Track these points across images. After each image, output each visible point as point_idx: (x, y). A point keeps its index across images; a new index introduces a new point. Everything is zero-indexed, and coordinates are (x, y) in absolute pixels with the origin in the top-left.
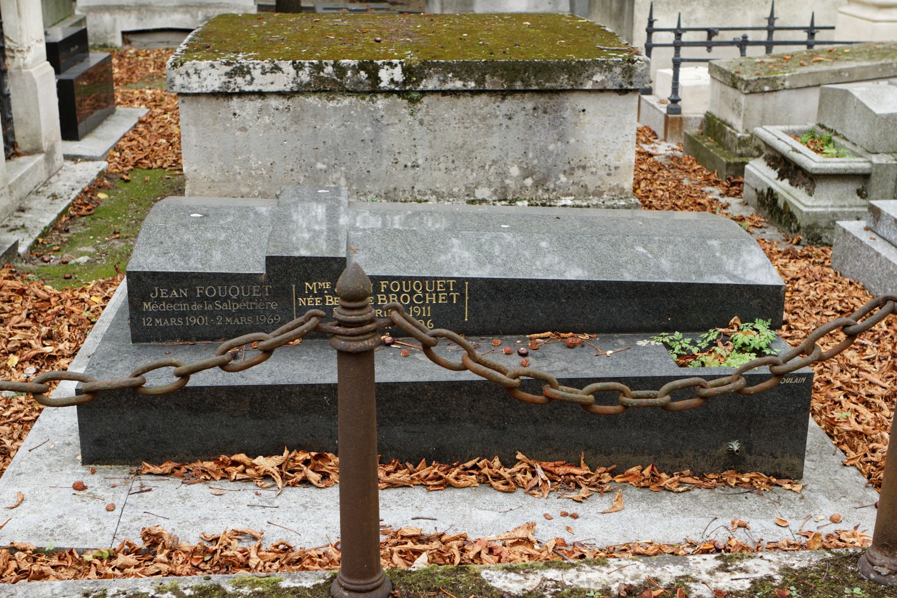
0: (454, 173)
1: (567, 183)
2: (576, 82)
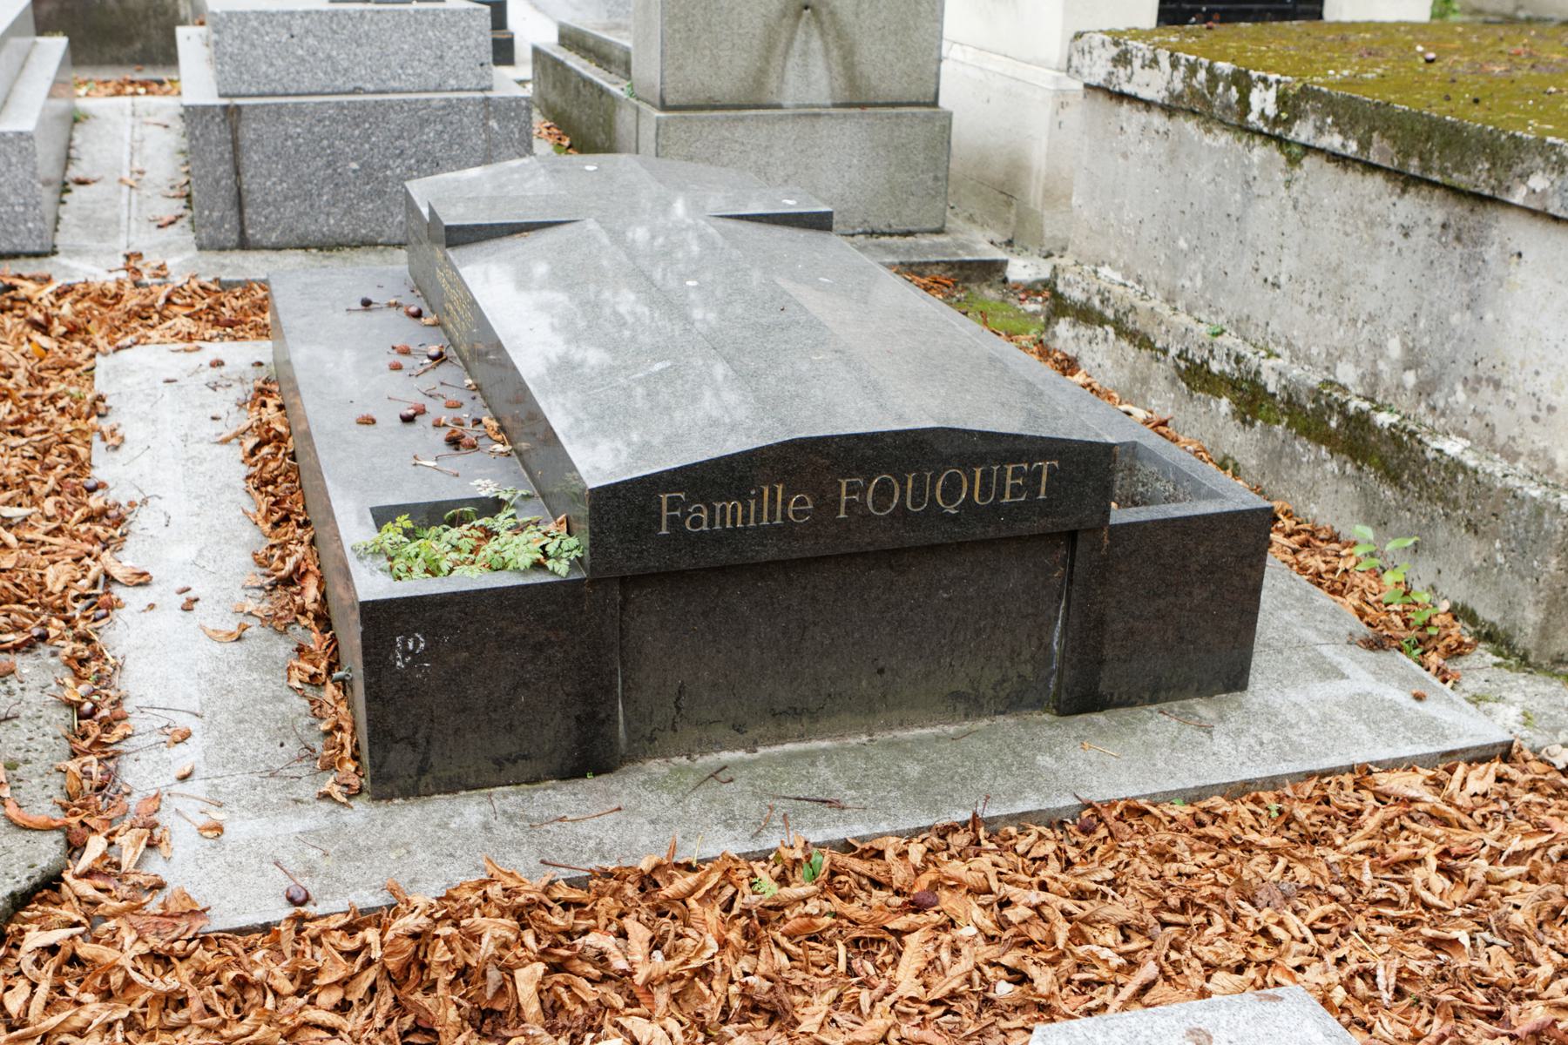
0: (1318, 317)
1: (1466, 407)
2: (1500, 182)
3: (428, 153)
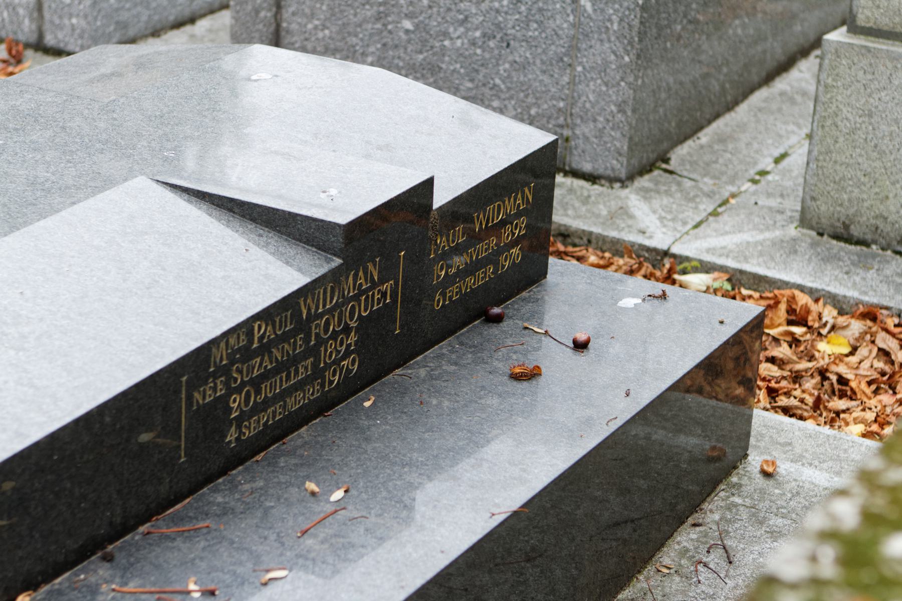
3: (498, 25)
